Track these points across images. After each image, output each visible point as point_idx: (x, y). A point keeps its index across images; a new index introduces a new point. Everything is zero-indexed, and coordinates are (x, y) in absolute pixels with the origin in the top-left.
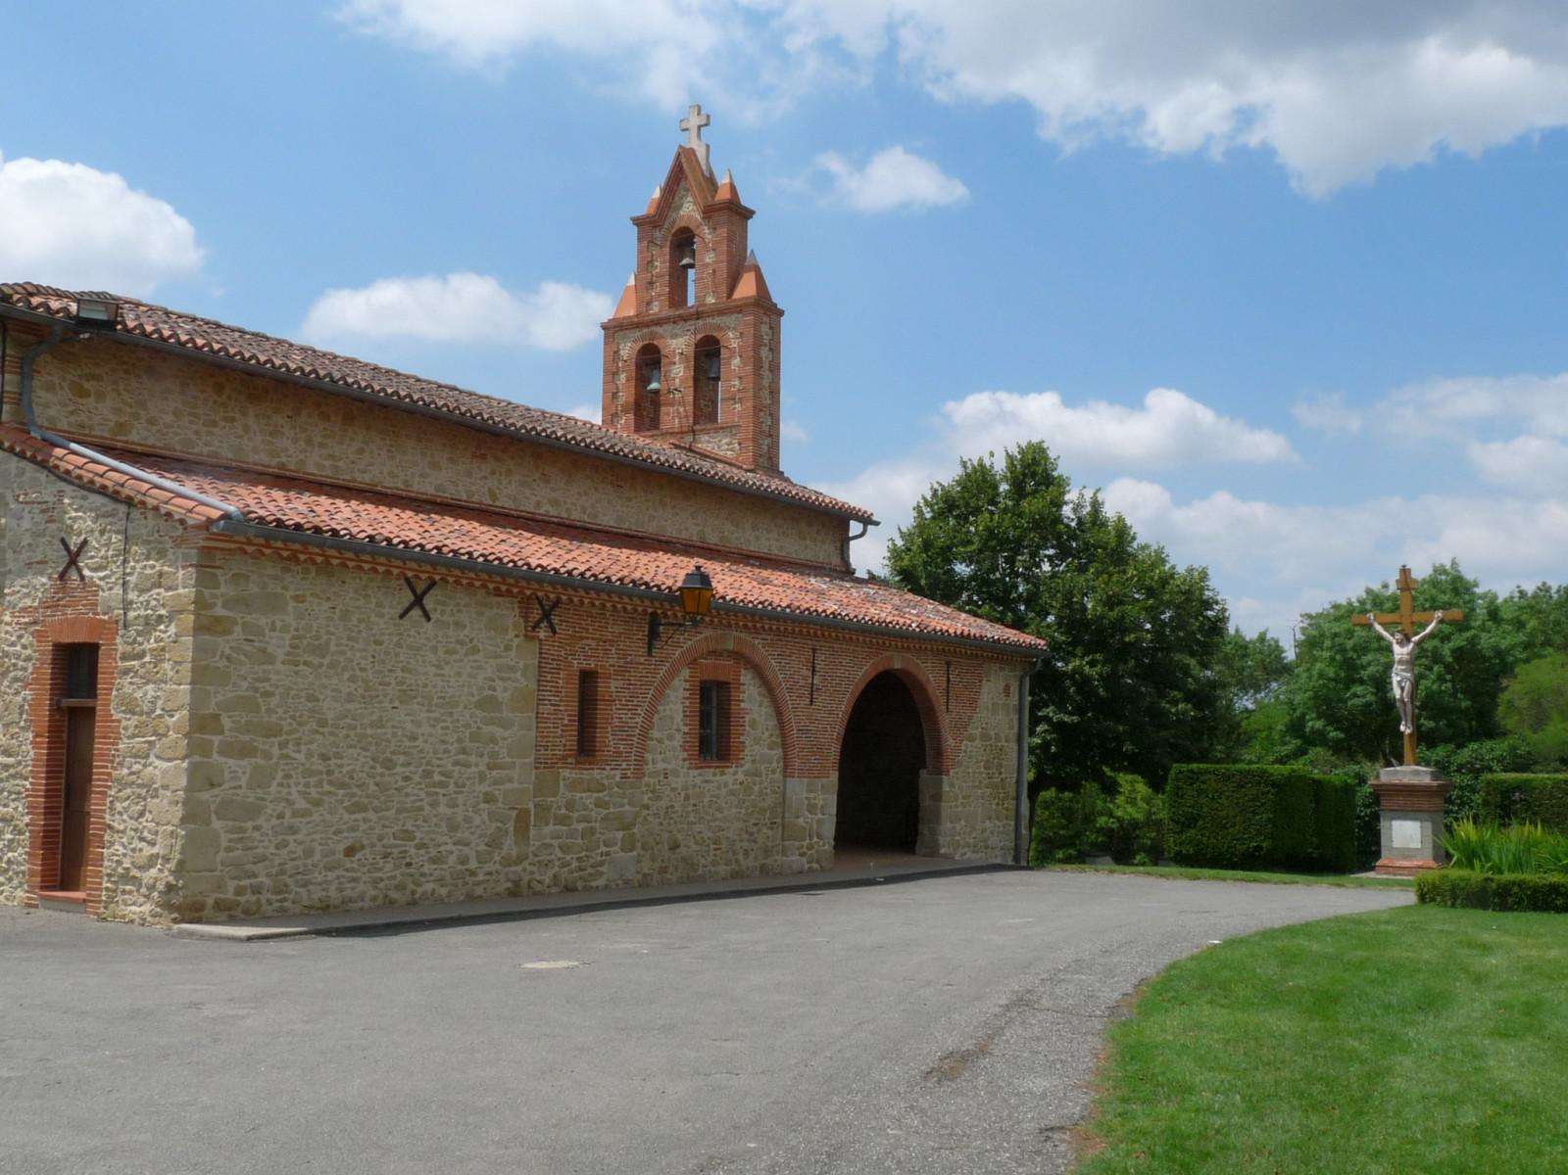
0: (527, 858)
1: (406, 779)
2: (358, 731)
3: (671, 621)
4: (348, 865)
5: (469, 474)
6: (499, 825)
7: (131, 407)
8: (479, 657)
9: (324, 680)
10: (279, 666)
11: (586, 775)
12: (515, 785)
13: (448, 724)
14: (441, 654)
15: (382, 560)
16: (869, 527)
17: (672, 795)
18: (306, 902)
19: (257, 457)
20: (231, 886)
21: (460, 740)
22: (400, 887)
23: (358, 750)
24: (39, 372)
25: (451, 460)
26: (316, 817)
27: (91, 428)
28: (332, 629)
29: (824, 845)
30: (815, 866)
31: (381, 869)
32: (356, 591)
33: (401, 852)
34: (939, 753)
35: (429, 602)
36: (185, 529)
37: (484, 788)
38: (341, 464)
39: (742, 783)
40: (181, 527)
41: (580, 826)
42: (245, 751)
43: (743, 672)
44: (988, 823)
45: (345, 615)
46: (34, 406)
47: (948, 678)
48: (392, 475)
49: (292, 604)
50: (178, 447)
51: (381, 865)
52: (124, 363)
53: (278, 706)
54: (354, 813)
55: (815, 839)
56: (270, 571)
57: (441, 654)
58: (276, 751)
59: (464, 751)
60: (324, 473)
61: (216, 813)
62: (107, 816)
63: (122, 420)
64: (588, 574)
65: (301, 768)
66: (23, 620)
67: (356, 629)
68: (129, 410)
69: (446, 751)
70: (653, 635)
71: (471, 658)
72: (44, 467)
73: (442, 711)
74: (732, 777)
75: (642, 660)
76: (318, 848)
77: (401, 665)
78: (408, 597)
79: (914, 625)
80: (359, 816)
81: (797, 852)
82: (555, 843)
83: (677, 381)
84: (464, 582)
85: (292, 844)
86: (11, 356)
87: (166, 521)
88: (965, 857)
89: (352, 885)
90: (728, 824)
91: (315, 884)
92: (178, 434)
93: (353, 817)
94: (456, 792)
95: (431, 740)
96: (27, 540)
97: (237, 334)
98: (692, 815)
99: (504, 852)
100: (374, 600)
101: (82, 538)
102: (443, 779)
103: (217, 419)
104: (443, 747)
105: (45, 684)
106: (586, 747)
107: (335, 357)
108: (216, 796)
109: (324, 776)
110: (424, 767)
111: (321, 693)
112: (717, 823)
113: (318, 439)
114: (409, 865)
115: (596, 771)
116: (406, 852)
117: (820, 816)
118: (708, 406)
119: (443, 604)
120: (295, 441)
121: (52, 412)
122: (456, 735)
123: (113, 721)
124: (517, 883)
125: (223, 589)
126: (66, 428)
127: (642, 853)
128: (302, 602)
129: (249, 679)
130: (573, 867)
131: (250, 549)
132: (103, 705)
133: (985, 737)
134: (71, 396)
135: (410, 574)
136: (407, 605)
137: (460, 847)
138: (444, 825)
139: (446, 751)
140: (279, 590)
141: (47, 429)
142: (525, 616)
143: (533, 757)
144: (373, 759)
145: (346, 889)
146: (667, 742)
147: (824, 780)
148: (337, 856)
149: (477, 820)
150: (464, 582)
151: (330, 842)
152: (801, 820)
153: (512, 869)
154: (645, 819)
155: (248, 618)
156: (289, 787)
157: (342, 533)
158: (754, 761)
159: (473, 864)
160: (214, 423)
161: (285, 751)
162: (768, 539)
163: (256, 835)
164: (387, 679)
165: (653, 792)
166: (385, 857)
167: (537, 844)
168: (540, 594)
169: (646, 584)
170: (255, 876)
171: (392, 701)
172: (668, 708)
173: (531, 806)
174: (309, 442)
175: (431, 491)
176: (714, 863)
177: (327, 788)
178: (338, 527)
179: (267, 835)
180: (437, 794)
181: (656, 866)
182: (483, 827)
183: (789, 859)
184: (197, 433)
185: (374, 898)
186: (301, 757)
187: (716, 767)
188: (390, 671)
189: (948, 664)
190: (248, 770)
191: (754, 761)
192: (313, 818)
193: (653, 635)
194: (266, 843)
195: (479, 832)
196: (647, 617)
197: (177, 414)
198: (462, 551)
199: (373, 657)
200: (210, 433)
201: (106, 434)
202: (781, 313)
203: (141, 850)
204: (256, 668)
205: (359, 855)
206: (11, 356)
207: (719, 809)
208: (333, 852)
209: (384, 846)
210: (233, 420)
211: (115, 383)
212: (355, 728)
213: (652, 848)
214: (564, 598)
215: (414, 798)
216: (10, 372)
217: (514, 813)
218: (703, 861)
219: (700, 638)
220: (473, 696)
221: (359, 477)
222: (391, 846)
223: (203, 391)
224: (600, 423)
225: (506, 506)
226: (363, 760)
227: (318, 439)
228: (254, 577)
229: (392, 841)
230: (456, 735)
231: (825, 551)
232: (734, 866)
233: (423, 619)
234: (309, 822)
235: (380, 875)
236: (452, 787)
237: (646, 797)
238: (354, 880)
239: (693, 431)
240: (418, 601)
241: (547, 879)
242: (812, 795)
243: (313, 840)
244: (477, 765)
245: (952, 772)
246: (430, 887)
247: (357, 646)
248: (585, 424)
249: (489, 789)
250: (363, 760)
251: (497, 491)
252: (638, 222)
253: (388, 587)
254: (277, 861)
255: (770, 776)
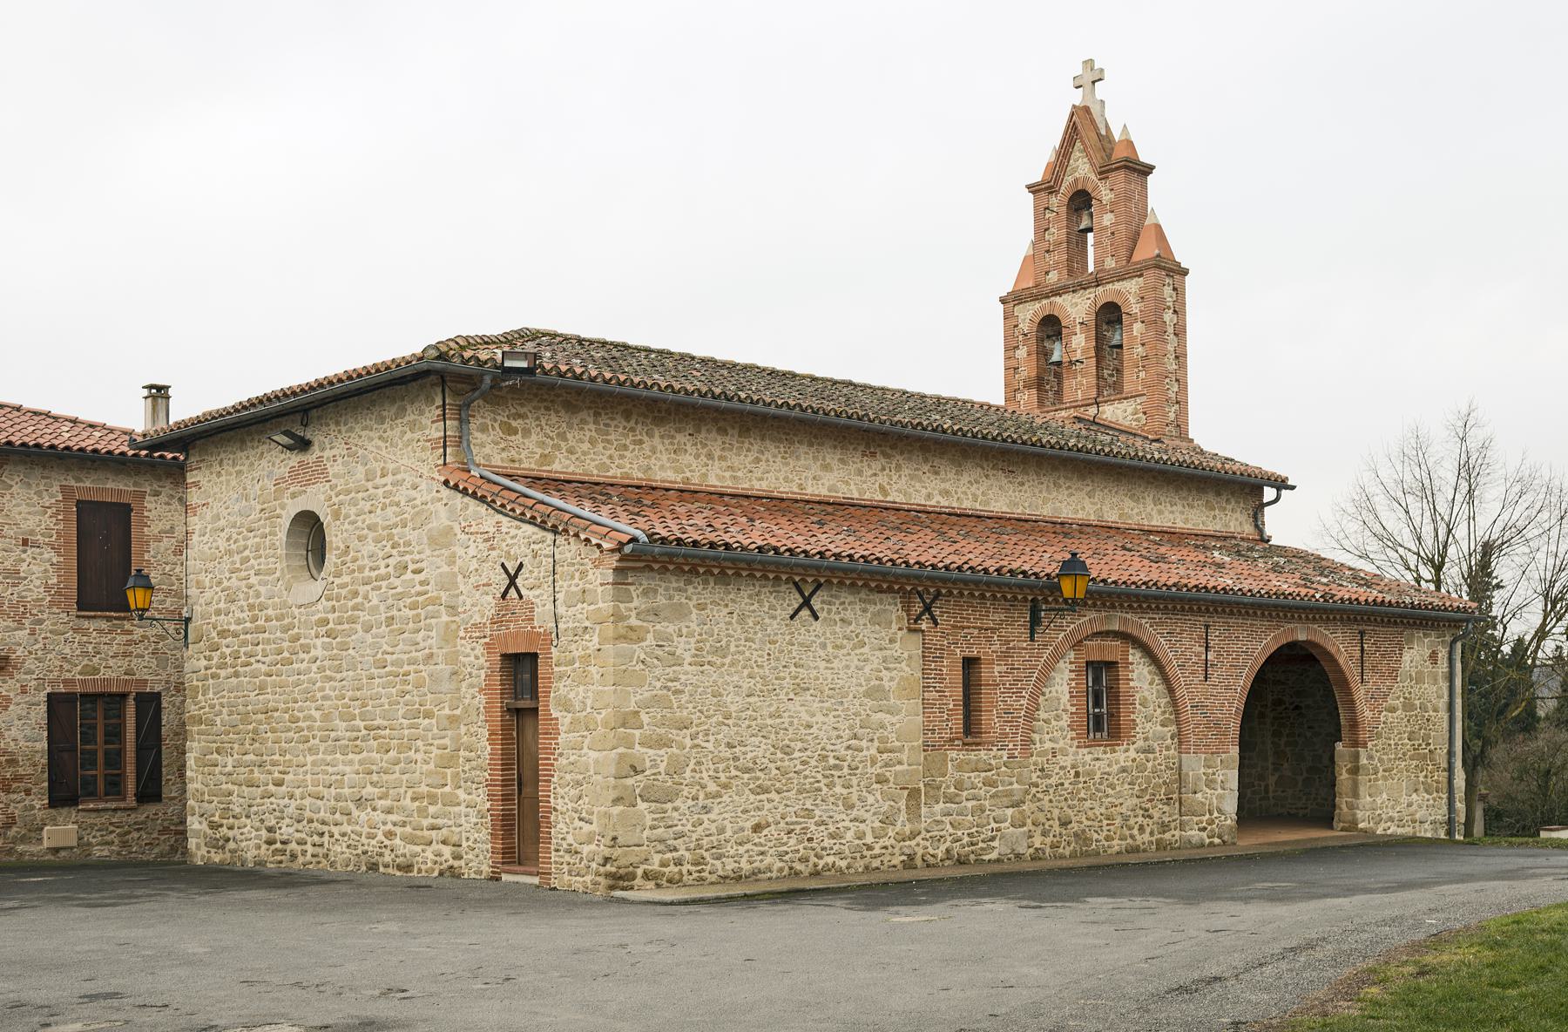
0: (919, 833)
1: (804, 763)
2: (759, 721)
3: (1053, 605)
4: (757, 840)
5: (860, 473)
6: (892, 803)
7: (552, 439)
8: (866, 650)
9: (726, 677)
10: (687, 667)
11: (972, 756)
12: (905, 767)
13: (839, 713)
14: (830, 649)
15: (772, 568)
16: (1284, 492)
17: (1062, 773)
18: (721, 873)
19: (664, 474)
20: (657, 858)
21: (851, 728)
22: (801, 860)
23: (760, 739)
24: (474, 416)
25: (842, 461)
26: (725, 798)
27: (520, 461)
28: (731, 631)
29: (1226, 819)
30: (1217, 841)
31: (785, 844)
32: (750, 597)
33: (803, 829)
34: (1354, 725)
35: (816, 603)
36: (601, 552)
37: (877, 770)
38: (740, 474)
39: (1134, 760)
40: (598, 551)
41: (970, 804)
42: (663, 743)
43: (1131, 651)
44: (1414, 796)
45: (742, 619)
46: (472, 446)
47: (1362, 647)
48: (786, 479)
49: (695, 611)
50: (595, 472)
51: (785, 840)
52: (545, 400)
53: (687, 702)
54: (758, 794)
55: (1216, 814)
56: (675, 585)
57: (830, 649)
58: (688, 742)
59: (855, 737)
60: (726, 484)
61: (640, 796)
62: (552, 800)
63: (546, 452)
64: (966, 566)
65: (710, 756)
66: (474, 635)
67: (752, 631)
68: (551, 443)
69: (839, 737)
70: (1035, 621)
71: (858, 651)
72: (484, 502)
73: (833, 701)
74: (1124, 755)
75: (1025, 645)
76: (729, 826)
77: (793, 661)
78: (796, 600)
79: (1318, 596)
80: (763, 797)
81: (1196, 827)
82: (947, 819)
83: (1079, 351)
84: (848, 582)
85: (706, 822)
86: (449, 404)
87: (586, 545)
88: (1389, 832)
89: (761, 857)
90: (1121, 800)
91: (728, 857)
92: (594, 460)
93: (759, 797)
94: (850, 774)
95: (824, 727)
96: (474, 565)
97: (643, 354)
98: (1083, 791)
99: (898, 828)
100: (767, 604)
101: (519, 562)
102: (837, 762)
103: (628, 442)
104: (836, 733)
105: (496, 689)
106: (971, 728)
107: (735, 365)
108: (641, 781)
109: (731, 762)
110: (819, 752)
111: (725, 690)
112: (1109, 799)
113: (717, 453)
114: (810, 840)
115: (982, 752)
116: (807, 828)
117: (1220, 791)
118: (1112, 375)
119: (830, 603)
120: (697, 456)
121: (487, 450)
122: (847, 723)
123: (552, 720)
124: (911, 857)
125: (636, 603)
126: (499, 463)
127: (1033, 828)
128: (703, 609)
129: (662, 680)
130: (964, 842)
131: (656, 566)
132: (544, 706)
133: (1408, 706)
134: (501, 435)
135: (797, 579)
136: (796, 606)
137: (857, 824)
138: (840, 803)
139: (839, 737)
140: (683, 600)
141: (484, 466)
142: (907, 608)
143: (921, 741)
144: (773, 746)
145: (756, 861)
146: (1054, 723)
147: (1223, 755)
148: (746, 833)
149: (871, 799)
150: (848, 582)
151: (739, 820)
152: (1199, 795)
153: (907, 843)
154: (1035, 795)
155: (658, 627)
156: (701, 772)
157: (734, 546)
158: (1146, 739)
159: (869, 839)
160: (625, 447)
161: (696, 742)
162: (1172, 512)
163: (675, 814)
164: (782, 674)
165: (1042, 770)
166: (789, 833)
167: (929, 821)
168: (920, 589)
169: (1024, 573)
170: (676, 850)
171: (787, 694)
172: (1053, 689)
173: (921, 785)
174: (710, 456)
175: (824, 492)
176: (1108, 838)
177: (734, 773)
178: (731, 541)
179: (685, 815)
180: (833, 776)
181: (1048, 840)
182: (876, 805)
183: (1188, 833)
184: (611, 457)
185: (781, 870)
186: (710, 746)
187: (1106, 746)
188: (785, 666)
189: (1362, 633)
190: (665, 758)
191: (1146, 739)
192: (723, 799)
193: (1035, 621)
194: (684, 821)
195: (873, 810)
196: (1029, 604)
197: (592, 442)
198: (843, 554)
199: (769, 654)
200: (622, 457)
201: (533, 466)
202: (1185, 272)
203: (581, 828)
204: (668, 670)
205: (765, 832)
206: (449, 404)
207: (1112, 786)
208: (742, 829)
209: (787, 823)
210: (641, 442)
211: (538, 419)
212: (756, 719)
213: (1043, 824)
214: (944, 591)
215: (812, 780)
216: (450, 419)
217: (906, 793)
218: (1095, 836)
219: (1088, 620)
220: (861, 685)
221: (757, 485)
222: (792, 823)
223: (612, 419)
224: (1002, 403)
225: (897, 500)
226: (765, 747)
227: (717, 453)
228: (661, 590)
229: (794, 819)
230: (847, 723)
231: (1237, 519)
232: (1129, 841)
233: (811, 619)
234: (720, 803)
235: (785, 848)
236: (846, 771)
237: (1034, 776)
238: (762, 853)
239: (1097, 403)
240: (806, 603)
241: (940, 853)
242: (1210, 771)
243: (724, 819)
244: (868, 748)
245: (1370, 745)
246: (830, 860)
247: (754, 646)
248: (982, 406)
249: (879, 771)
250: (765, 747)
251: (888, 487)
252: (1034, 189)
253: (778, 592)
254: (695, 836)
255: (1164, 752)
